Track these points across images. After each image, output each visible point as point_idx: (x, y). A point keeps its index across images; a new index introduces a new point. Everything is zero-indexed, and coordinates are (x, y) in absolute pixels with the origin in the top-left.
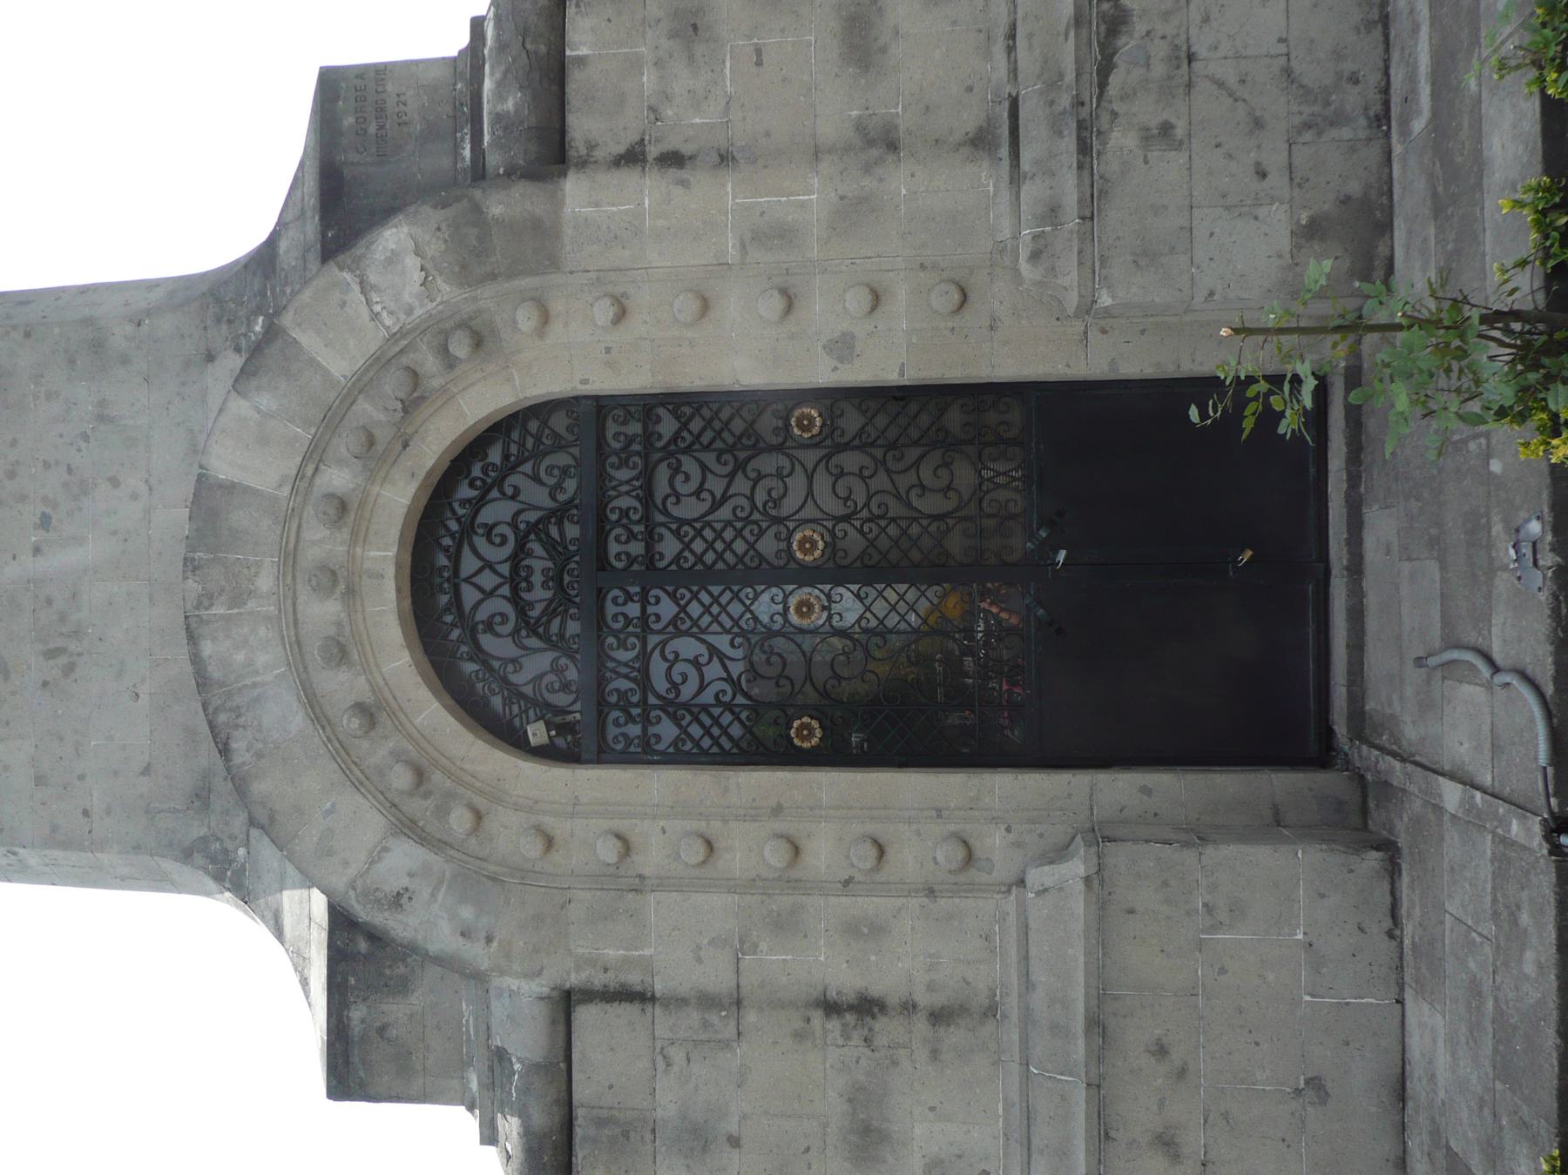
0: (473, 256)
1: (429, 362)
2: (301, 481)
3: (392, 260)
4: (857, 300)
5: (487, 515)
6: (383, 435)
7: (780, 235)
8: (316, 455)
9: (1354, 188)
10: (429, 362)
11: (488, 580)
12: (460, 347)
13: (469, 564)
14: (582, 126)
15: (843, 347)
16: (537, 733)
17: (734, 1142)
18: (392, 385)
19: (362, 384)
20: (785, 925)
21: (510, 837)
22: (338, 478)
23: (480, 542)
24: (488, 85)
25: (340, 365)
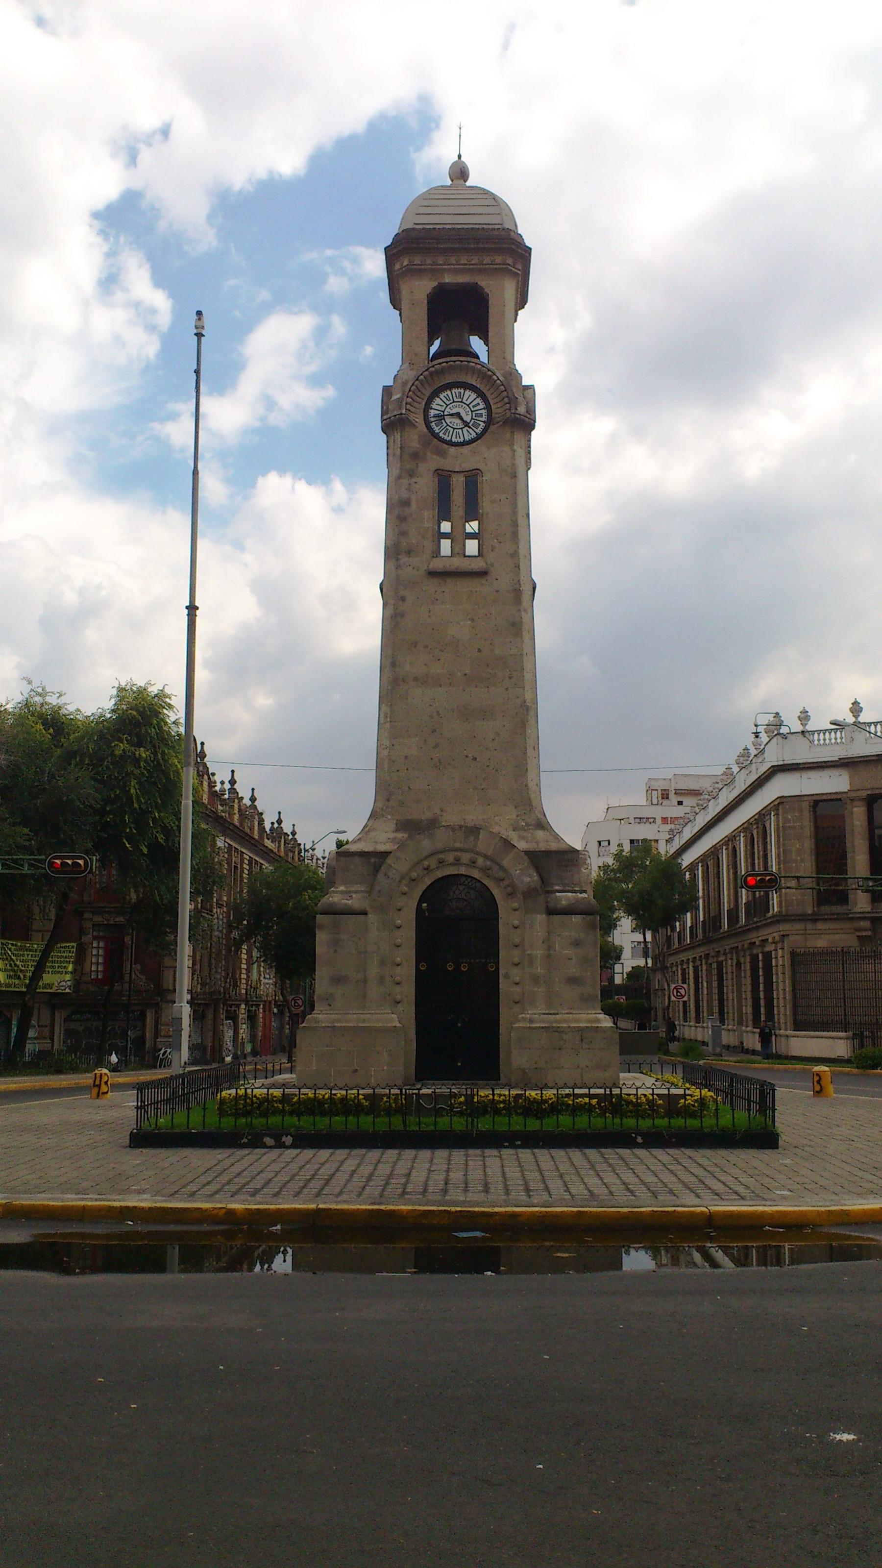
0: (529, 894)
1: (505, 883)
2: (478, 853)
3: (530, 876)
4: (517, 979)
5: (472, 892)
6: (490, 872)
7: (531, 963)
8: (486, 857)
9: (643, 1252)
10: (505, 883)
11: (457, 892)
12: (509, 889)
13: (461, 888)
14: (557, 919)
15: (507, 976)
16: (640, 1140)
17: (335, 951)
18: (501, 874)
19: (501, 867)
20: (382, 963)
21: (401, 901)
22: (480, 861)
23: (466, 890)
24: (570, 894)
25: (505, 863)
